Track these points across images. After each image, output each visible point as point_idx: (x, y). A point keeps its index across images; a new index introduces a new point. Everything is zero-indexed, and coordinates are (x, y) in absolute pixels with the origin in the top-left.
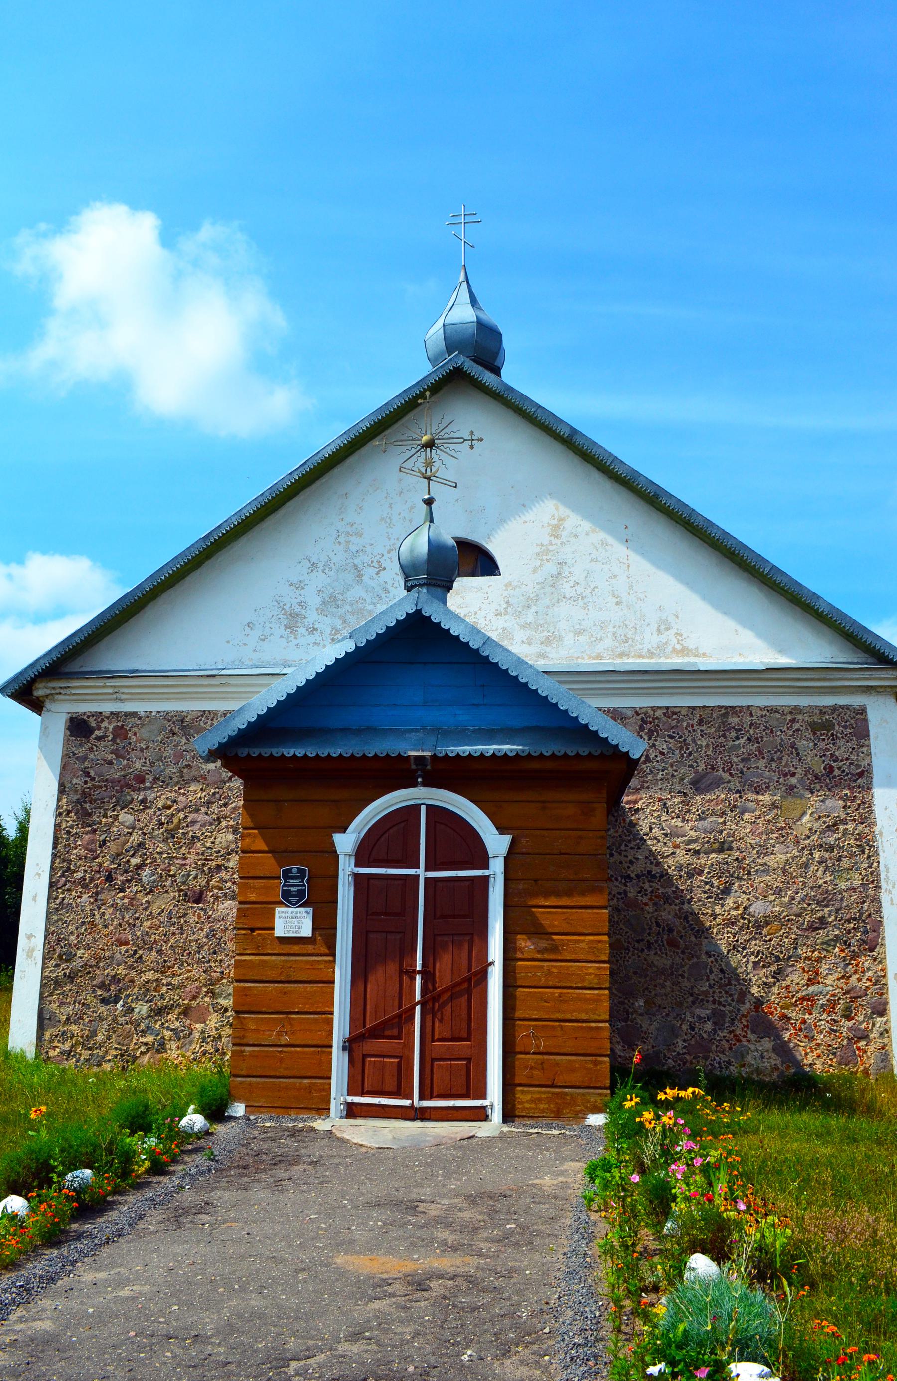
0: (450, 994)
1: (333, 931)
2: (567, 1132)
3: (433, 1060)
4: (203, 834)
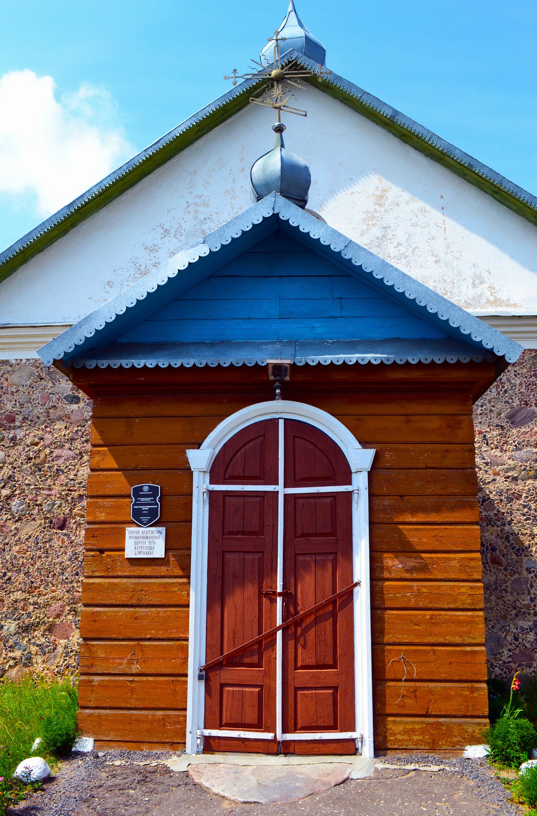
0: (312, 618)
1: (186, 552)
2: (447, 768)
3: (296, 689)
4: (67, 467)
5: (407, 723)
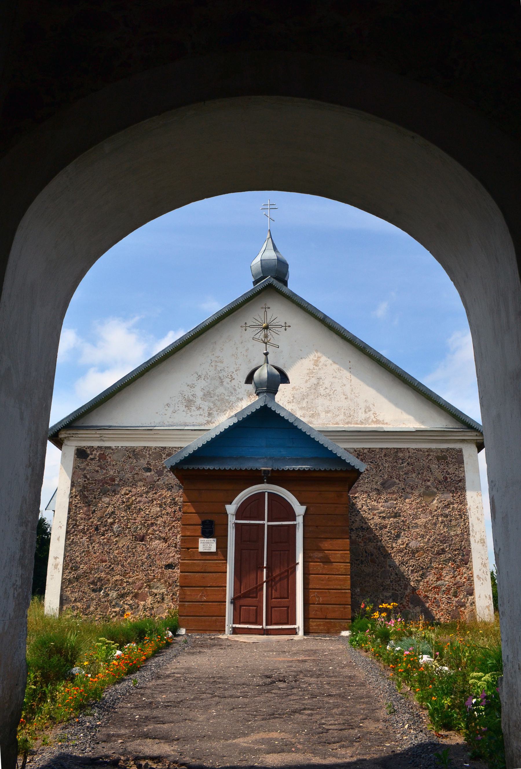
3: (272, 607)
5: (317, 622)
